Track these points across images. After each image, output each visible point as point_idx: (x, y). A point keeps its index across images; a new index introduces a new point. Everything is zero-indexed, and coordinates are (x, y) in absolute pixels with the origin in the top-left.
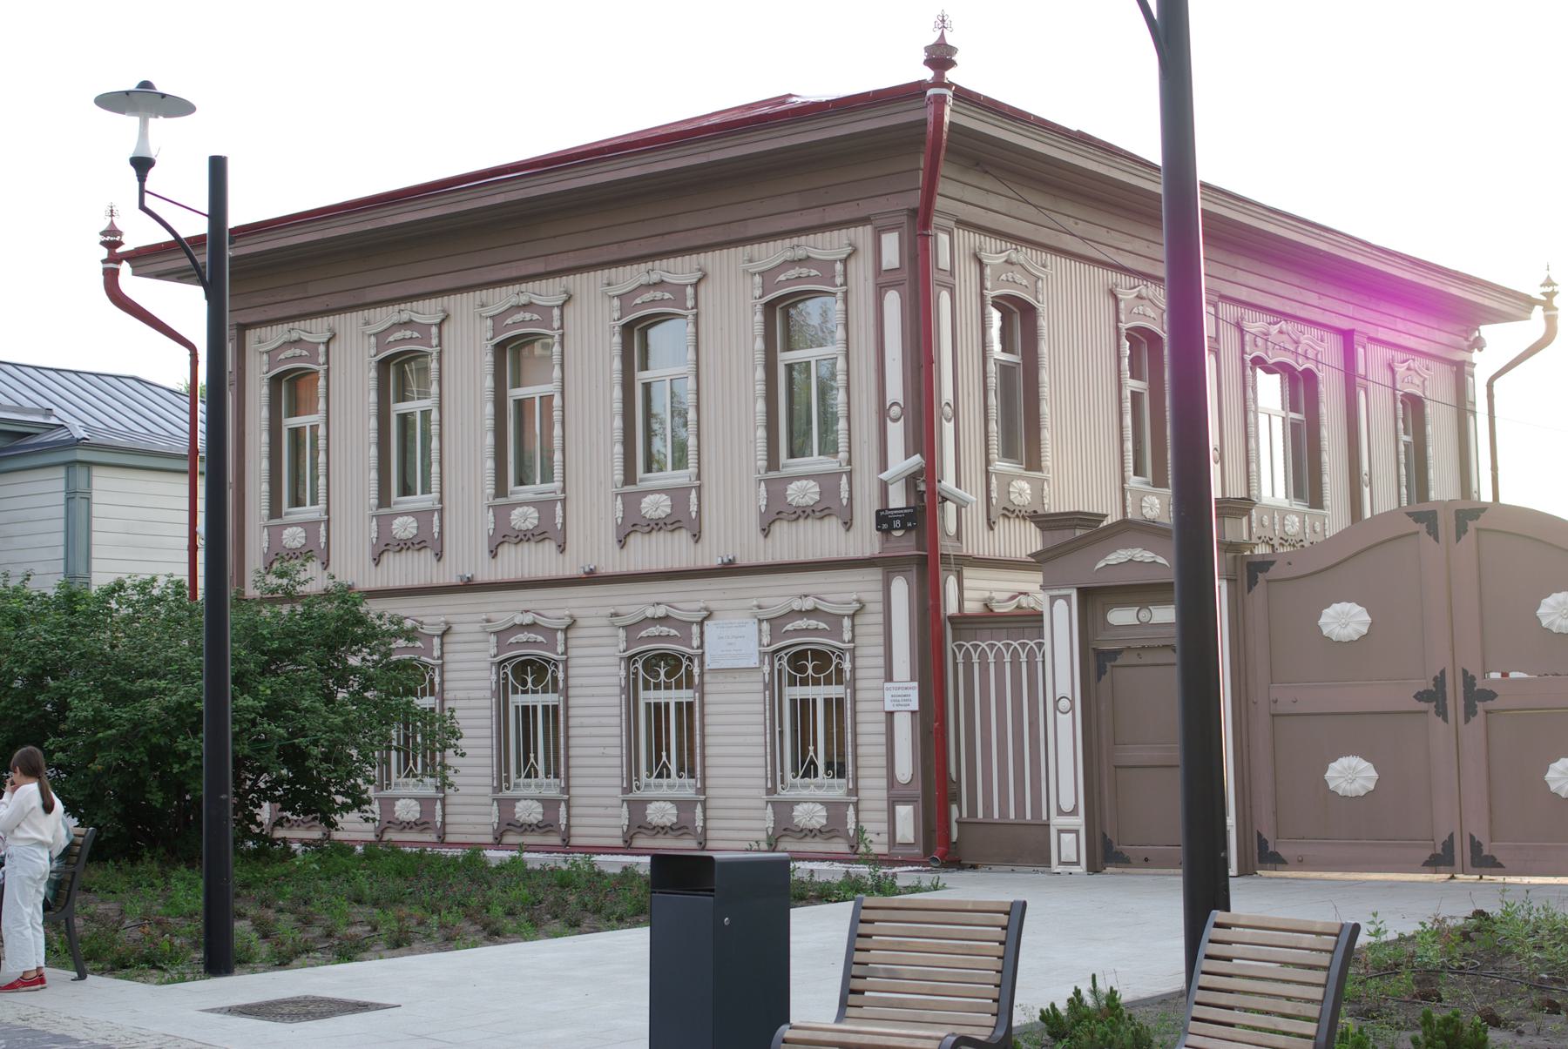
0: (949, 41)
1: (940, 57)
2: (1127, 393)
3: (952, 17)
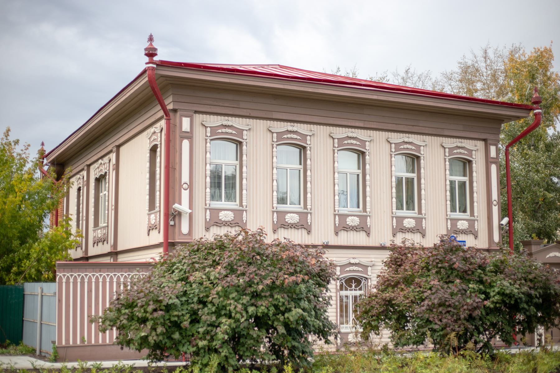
1: (151, 53)
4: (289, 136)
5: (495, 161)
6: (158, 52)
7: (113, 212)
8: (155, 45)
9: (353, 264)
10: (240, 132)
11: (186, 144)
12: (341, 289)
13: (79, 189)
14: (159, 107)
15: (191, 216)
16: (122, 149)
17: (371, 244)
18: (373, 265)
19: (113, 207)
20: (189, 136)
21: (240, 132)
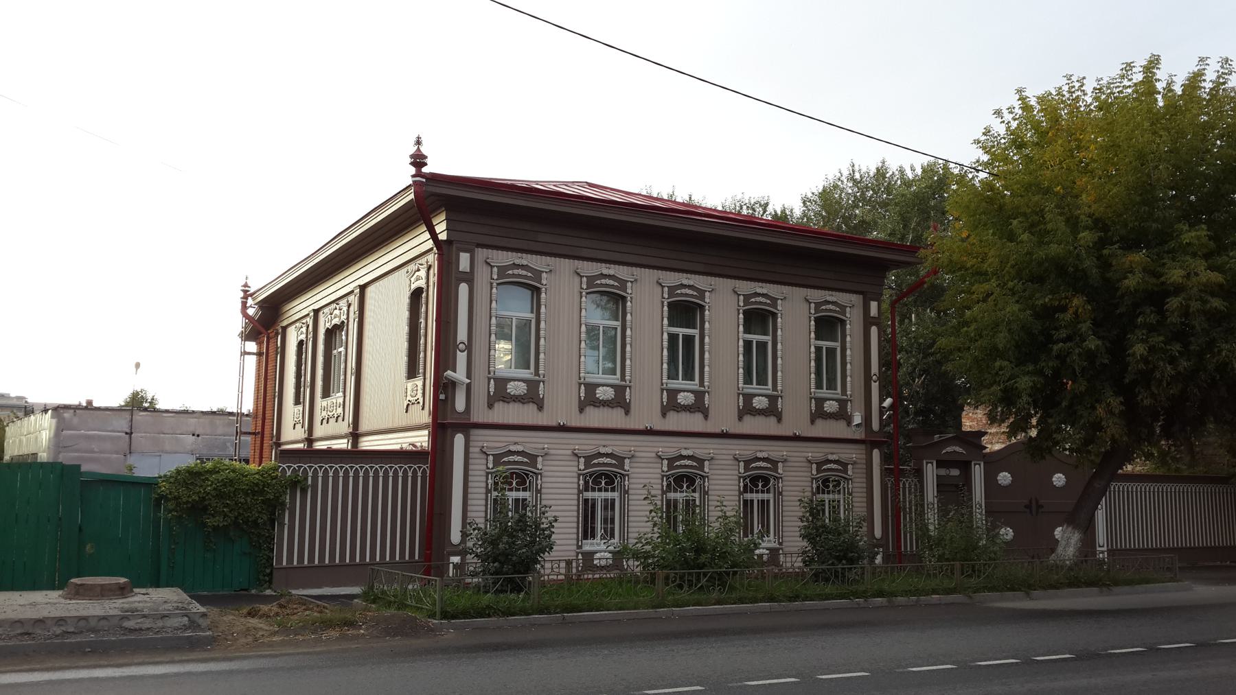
1: (418, 161)
4: (603, 281)
5: (876, 322)
6: (428, 161)
8: (424, 150)
10: (538, 274)
11: (463, 288)
12: (745, 491)
13: (301, 344)
14: (427, 235)
15: (469, 386)
17: (545, 423)
18: (786, 461)
20: (469, 278)
21: (538, 274)
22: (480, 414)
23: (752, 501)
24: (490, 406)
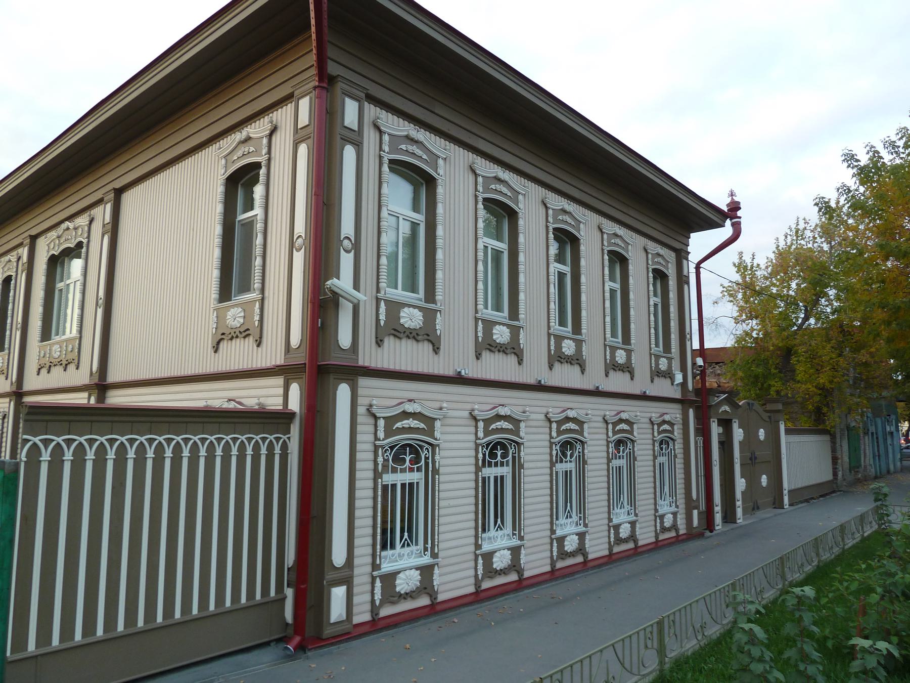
0: (736, 199)
2: (652, 303)
3: (736, 191)
7: (19, 333)
9: (410, 413)
11: (349, 153)
16: (128, 198)
18: (445, 417)
19: (19, 326)
22: (369, 357)
23: (394, 486)
24: (379, 342)
